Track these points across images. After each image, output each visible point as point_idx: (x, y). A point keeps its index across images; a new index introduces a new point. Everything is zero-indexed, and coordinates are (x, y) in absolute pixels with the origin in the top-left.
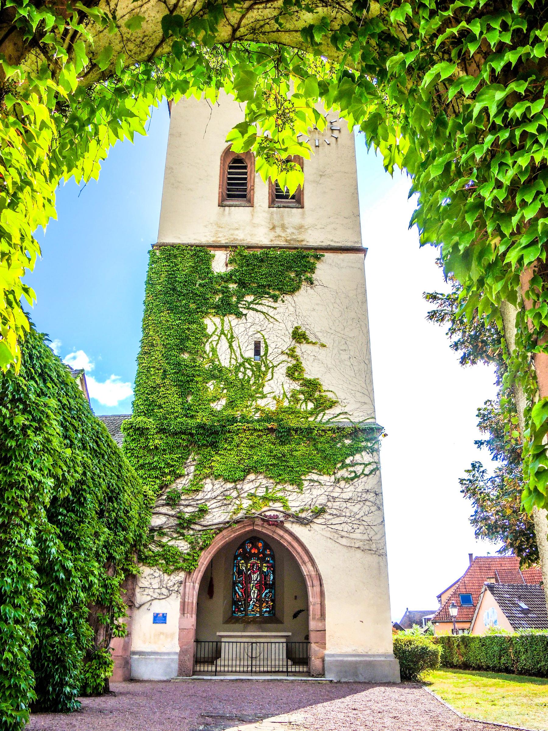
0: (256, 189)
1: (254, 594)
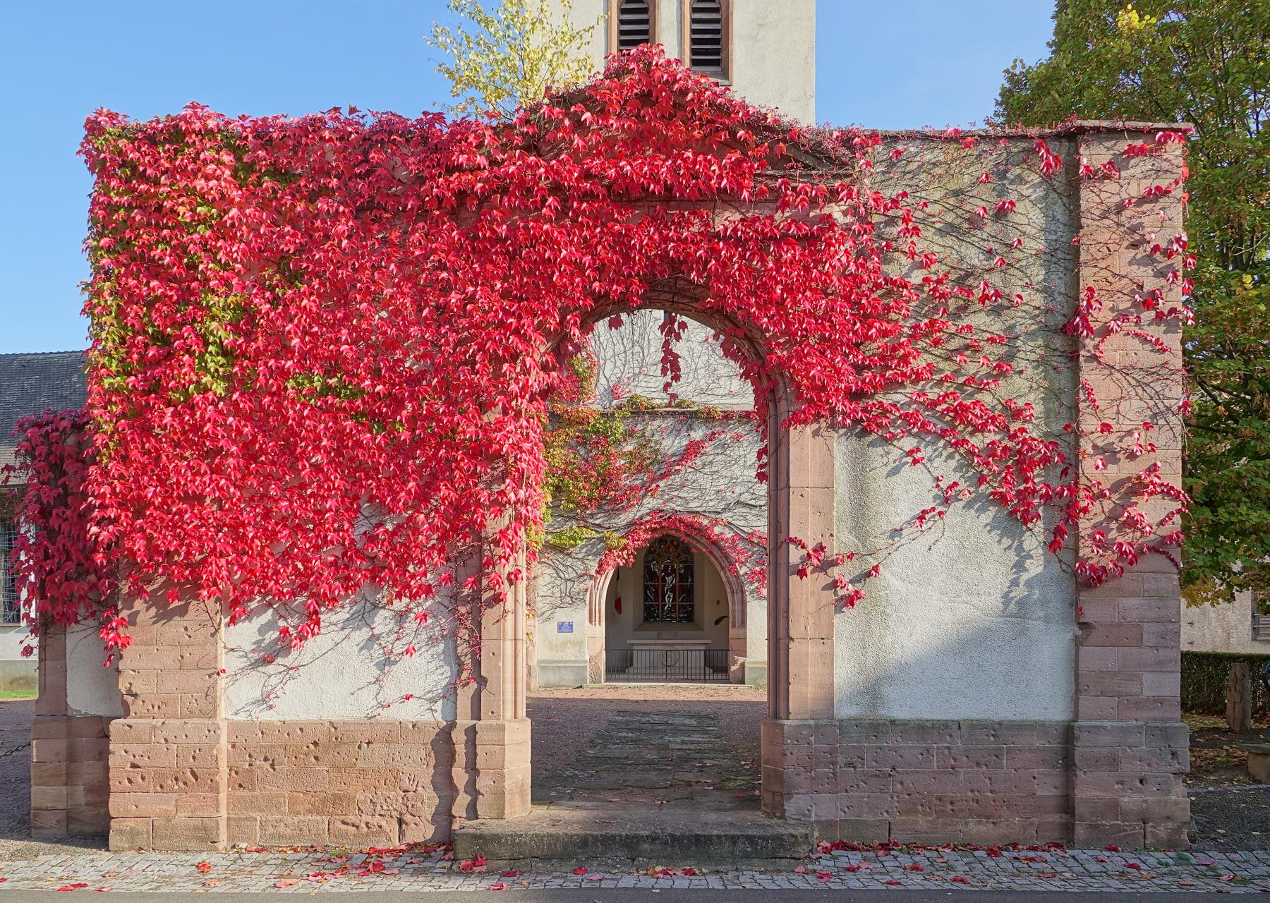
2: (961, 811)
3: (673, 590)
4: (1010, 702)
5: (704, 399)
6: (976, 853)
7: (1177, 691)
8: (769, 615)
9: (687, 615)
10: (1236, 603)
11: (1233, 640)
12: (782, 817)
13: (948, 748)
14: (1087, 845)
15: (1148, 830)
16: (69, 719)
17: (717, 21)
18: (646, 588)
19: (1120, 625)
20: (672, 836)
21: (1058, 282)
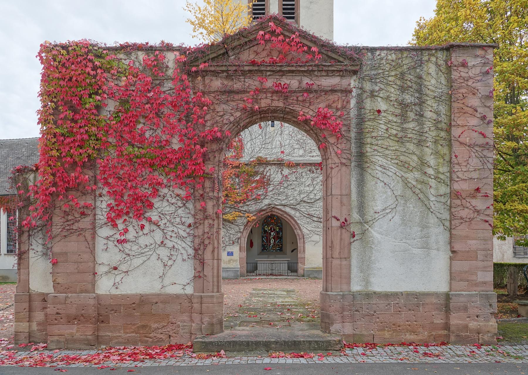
0: (64, 41)
1: (272, 241)
2: (403, 329)
3: (274, 238)
4: (423, 284)
5: (288, 158)
6: (410, 347)
7: (492, 279)
8: (323, 248)
9: (281, 249)
10: (506, 241)
11: (505, 257)
13: (397, 303)
14: (455, 343)
15: (480, 337)
18: (263, 237)
19: (468, 252)
20: (284, 341)
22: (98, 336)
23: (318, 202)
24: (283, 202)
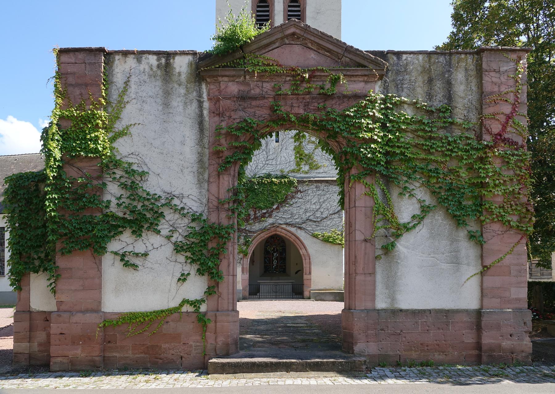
12: (353, 353)
16: (30, 312)
17: (299, 11)
18: (265, 258)
21: (473, 117)
22: (104, 357)
23: (325, 220)
24: (288, 221)
